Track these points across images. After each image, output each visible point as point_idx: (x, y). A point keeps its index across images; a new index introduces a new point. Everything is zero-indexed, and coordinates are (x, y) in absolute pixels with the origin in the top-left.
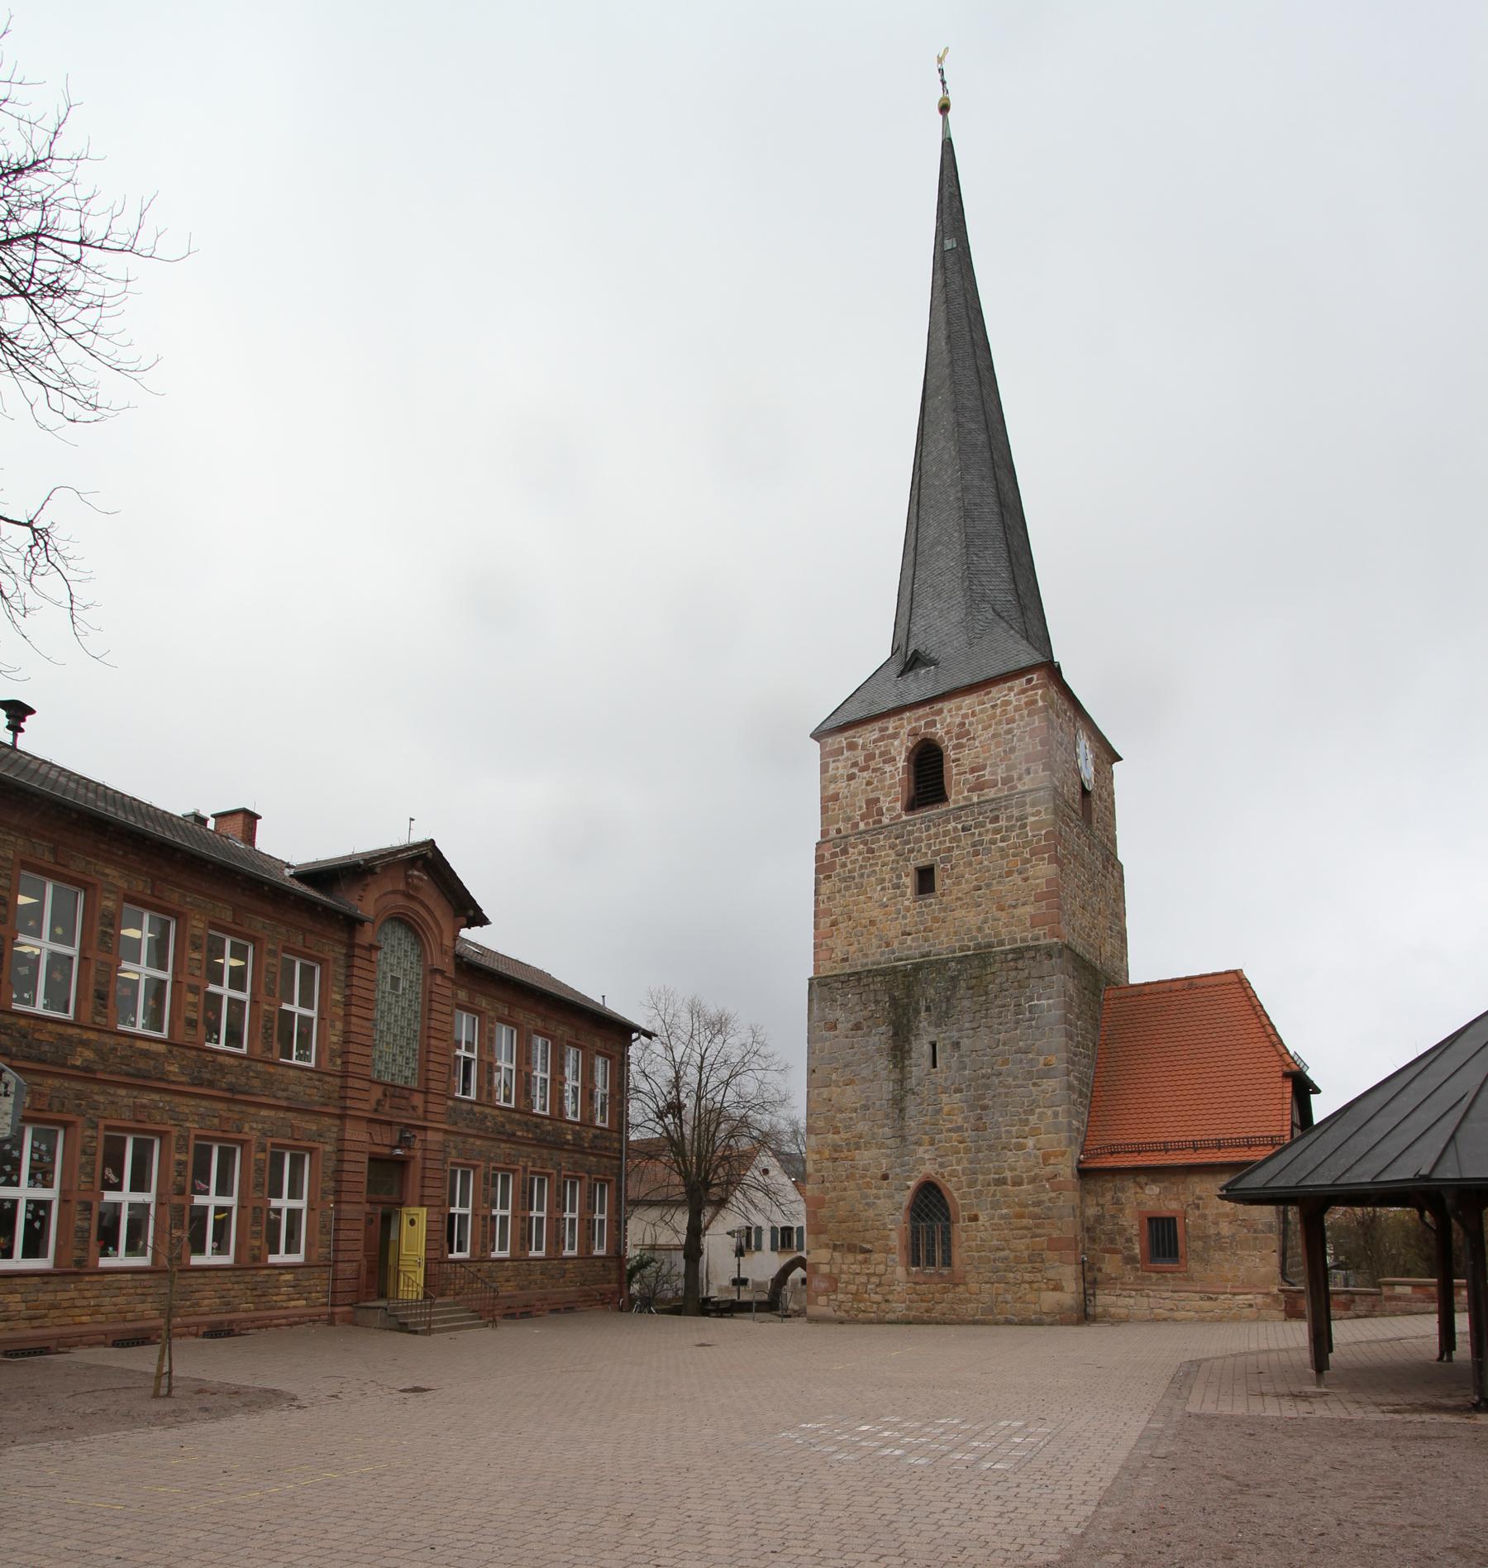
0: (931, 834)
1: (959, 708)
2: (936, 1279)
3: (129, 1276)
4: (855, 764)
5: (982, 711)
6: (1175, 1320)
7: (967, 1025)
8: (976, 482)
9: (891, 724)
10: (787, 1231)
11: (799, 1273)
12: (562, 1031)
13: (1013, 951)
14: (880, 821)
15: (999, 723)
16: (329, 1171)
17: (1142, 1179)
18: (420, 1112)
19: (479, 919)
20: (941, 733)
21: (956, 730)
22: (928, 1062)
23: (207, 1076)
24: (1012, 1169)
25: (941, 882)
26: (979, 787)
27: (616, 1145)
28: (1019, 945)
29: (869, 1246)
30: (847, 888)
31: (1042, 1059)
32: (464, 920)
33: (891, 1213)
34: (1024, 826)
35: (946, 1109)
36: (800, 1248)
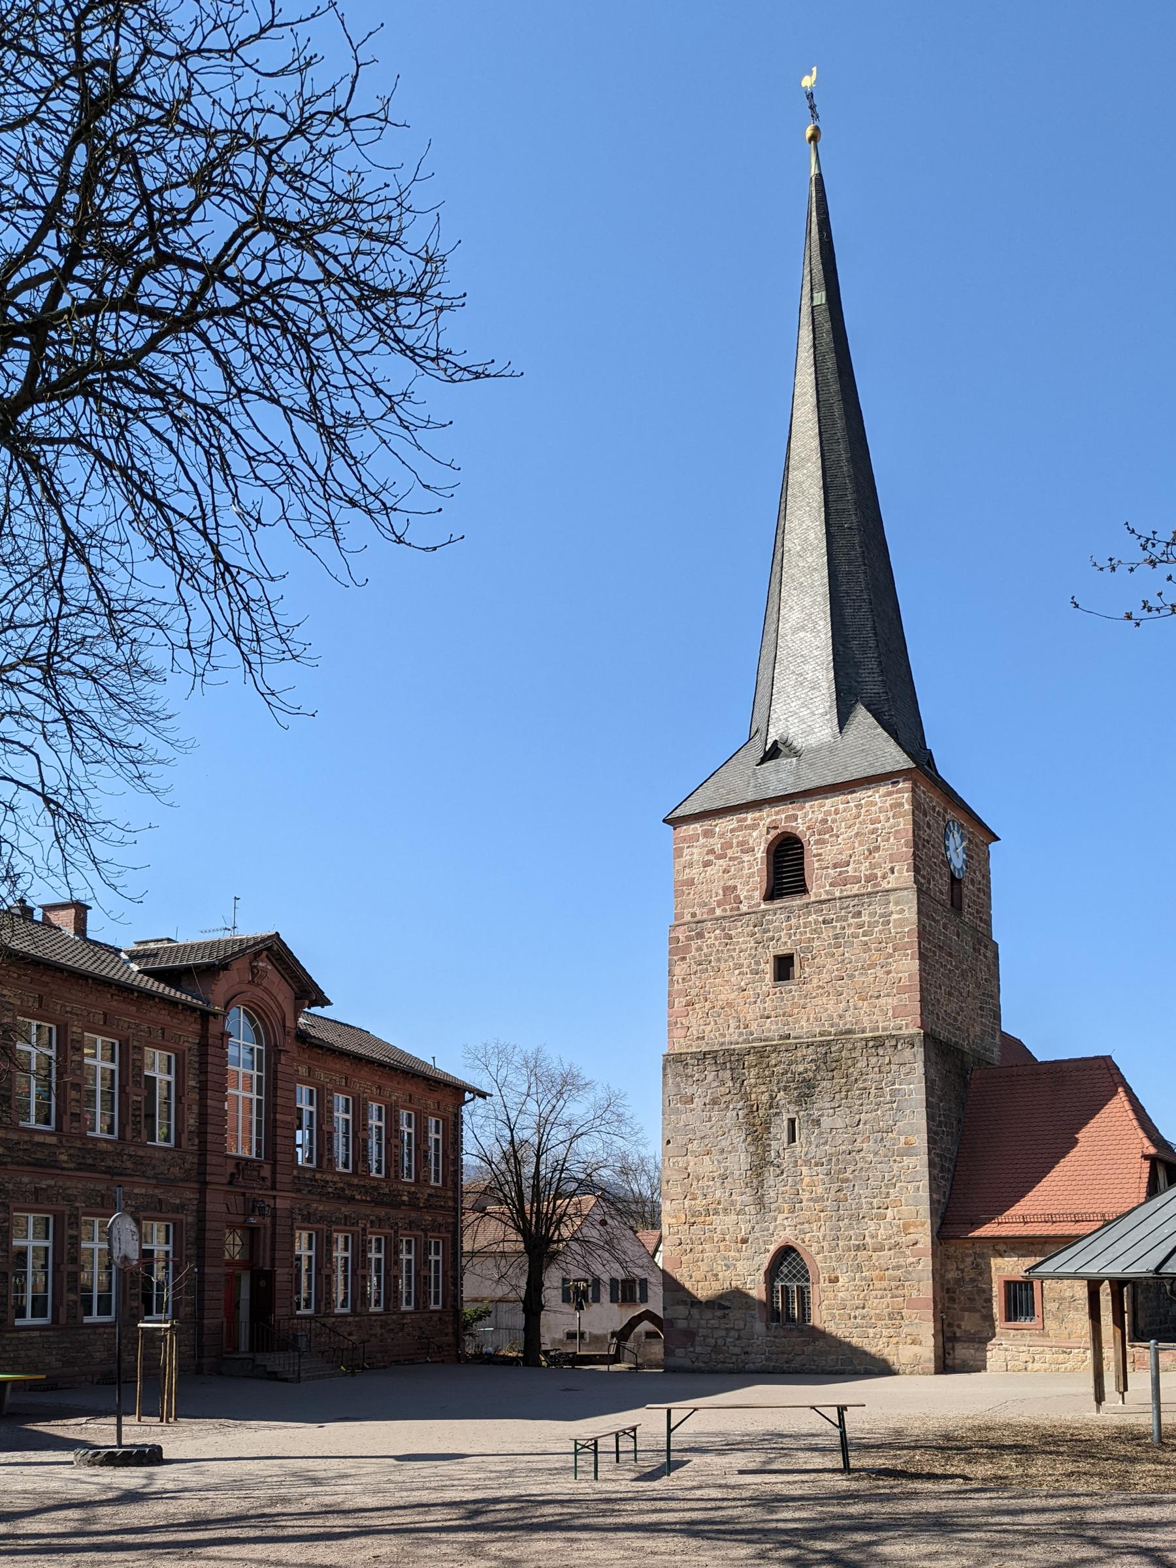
0: (789, 925)
2: (795, 1333)
3: (37, 1333)
4: (712, 851)
7: (828, 1105)
11: (646, 1326)
13: (874, 1038)
18: (269, 1183)
20: (802, 828)
22: (785, 1137)
23: (90, 1161)
28: (880, 1033)
29: (727, 1304)
31: (902, 1138)
32: (307, 1002)
34: (888, 922)
36: (644, 1299)
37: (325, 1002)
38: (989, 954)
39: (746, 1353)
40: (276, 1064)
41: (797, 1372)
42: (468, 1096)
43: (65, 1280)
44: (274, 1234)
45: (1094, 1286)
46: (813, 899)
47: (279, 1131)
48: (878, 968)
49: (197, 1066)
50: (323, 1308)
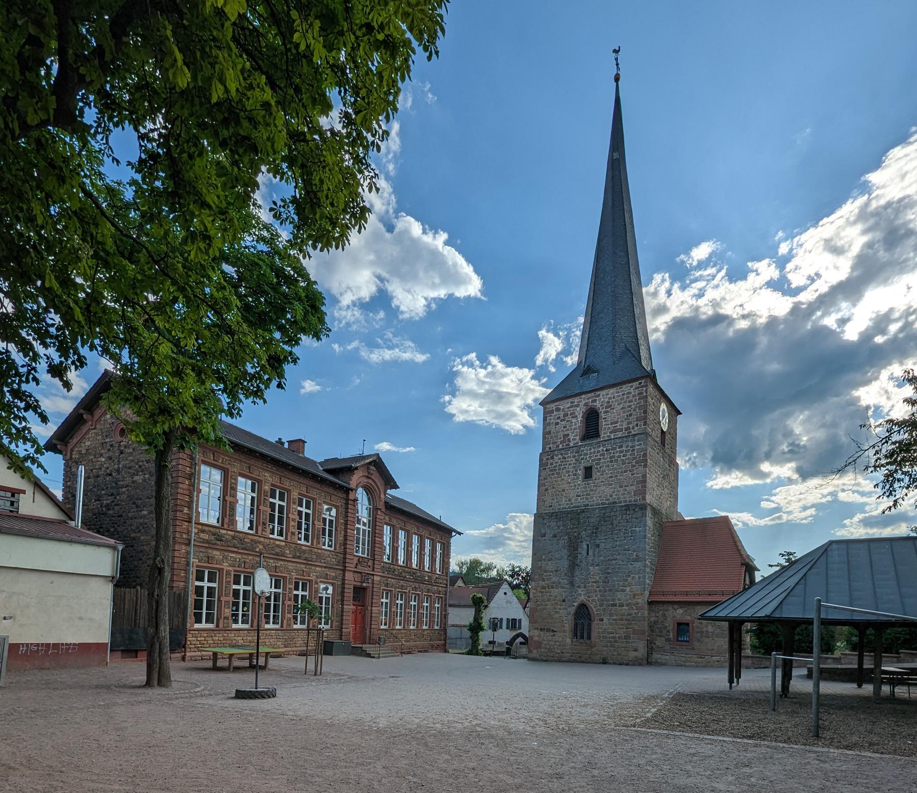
0: (591, 453)
1: (607, 394)
9: (576, 400)
10: (514, 620)
11: (520, 639)
12: (425, 533)
17: (676, 606)
19: (396, 487)
20: (599, 405)
21: (605, 405)
22: (585, 554)
33: (565, 617)
36: (520, 628)
42: (454, 534)
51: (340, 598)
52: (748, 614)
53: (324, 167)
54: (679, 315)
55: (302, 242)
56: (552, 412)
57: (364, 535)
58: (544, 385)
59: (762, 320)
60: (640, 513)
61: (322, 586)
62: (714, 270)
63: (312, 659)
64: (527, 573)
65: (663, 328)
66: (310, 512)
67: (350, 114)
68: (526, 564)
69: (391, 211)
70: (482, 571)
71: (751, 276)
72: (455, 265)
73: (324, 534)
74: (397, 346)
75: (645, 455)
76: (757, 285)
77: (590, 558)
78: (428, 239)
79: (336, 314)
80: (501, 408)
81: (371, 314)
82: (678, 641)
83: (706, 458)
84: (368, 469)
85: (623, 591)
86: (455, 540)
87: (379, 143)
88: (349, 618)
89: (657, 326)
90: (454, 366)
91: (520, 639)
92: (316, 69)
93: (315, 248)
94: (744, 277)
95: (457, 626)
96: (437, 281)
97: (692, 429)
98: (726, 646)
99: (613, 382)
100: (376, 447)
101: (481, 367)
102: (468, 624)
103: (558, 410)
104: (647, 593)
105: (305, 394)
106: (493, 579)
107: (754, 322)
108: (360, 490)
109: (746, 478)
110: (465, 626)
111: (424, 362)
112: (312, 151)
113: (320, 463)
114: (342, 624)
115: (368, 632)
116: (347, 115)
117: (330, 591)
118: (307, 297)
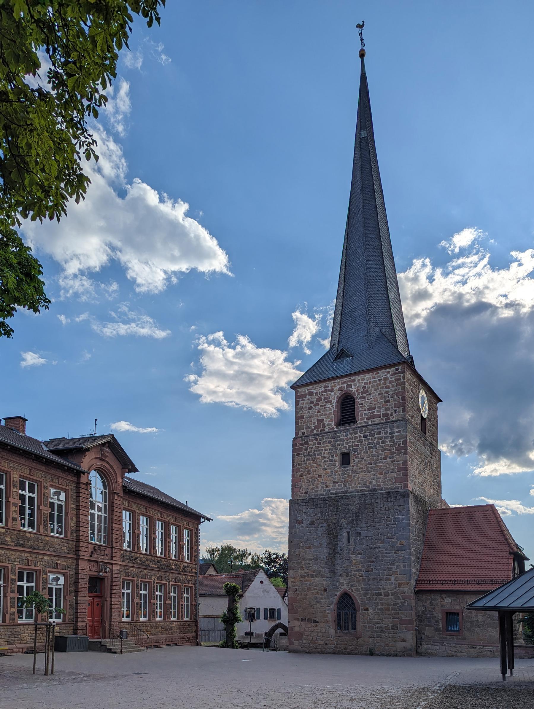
0: (348, 438)
1: (363, 379)
5: (374, 382)
6: (457, 656)
7: (364, 525)
8: (374, 266)
9: (330, 385)
10: (272, 610)
11: (280, 630)
12: (169, 519)
14: (324, 430)
15: (382, 388)
16: (72, 583)
17: (444, 596)
19: (134, 470)
20: (354, 391)
21: (361, 390)
22: (346, 542)
23: (21, 542)
24: (384, 589)
25: (353, 461)
26: (371, 417)
27: (194, 570)
29: (318, 620)
30: (308, 460)
31: (399, 542)
32: (127, 470)
33: (328, 607)
34: (393, 437)
35: (354, 562)
36: (279, 618)
37: (135, 470)
38: (437, 456)
39: (326, 644)
40: (113, 499)
41: (349, 654)
42: (202, 520)
43: (9, 601)
44: (112, 581)
45: (52, 673)
46: (358, 425)
47: (114, 532)
48: (388, 459)
49: (75, 498)
50: (135, 619)
51: (73, 589)
52: (518, 604)
53: (31, 131)
54: (441, 301)
55: (10, 207)
56: (305, 396)
57: (99, 521)
58: (298, 368)
59: (525, 310)
60: (402, 501)
61: (52, 576)
62: (475, 258)
63: (41, 657)
64: (285, 561)
65: (424, 314)
66: (34, 496)
67: (61, 75)
68: (283, 550)
69: (122, 175)
70: (236, 558)
71: (514, 265)
72: (197, 237)
73: (52, 520)
74: (134, 321)
75: (405, 442)
76: (521, 275)
77: (352, 546)
78: (166, 208)
79: (61, 283)
80: (252, 390)
81: (103, 285)
82: (448, 630)
83: (472, 445)
84: (101, 450)
85: (388, 580)
86: (204, 527)
87: (96, 107)
88: (84, 611)
89: (415, 313)
90: (199, 344)
91: (280, 630)
92: (18, 24)
93: (25, 216)
94: (507, 267)
95: (209, 617)
96: (177, 253)
97: (454, 416)
98: (497, 636)
99: (368, 367)
100: (114, 426)
101: (229, 347)
102: (221, 614)
103: (311, 394)
104: (413, 582)
105: (26, 367)
106: (247, 567)
107: (517, 312)
108: (93, 473)
109: (514, 466)
110: (218, 617)
111: (164, 339)
112: (16, 112)
113: (45, 443)
114: (76, 617)
115: (107, 625)
116: (56, 75)
117: (62, 581)
118: (19, 263)
